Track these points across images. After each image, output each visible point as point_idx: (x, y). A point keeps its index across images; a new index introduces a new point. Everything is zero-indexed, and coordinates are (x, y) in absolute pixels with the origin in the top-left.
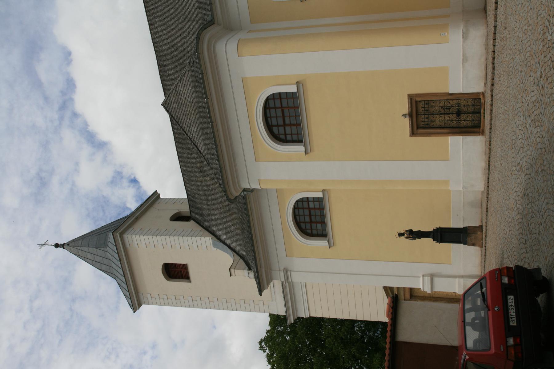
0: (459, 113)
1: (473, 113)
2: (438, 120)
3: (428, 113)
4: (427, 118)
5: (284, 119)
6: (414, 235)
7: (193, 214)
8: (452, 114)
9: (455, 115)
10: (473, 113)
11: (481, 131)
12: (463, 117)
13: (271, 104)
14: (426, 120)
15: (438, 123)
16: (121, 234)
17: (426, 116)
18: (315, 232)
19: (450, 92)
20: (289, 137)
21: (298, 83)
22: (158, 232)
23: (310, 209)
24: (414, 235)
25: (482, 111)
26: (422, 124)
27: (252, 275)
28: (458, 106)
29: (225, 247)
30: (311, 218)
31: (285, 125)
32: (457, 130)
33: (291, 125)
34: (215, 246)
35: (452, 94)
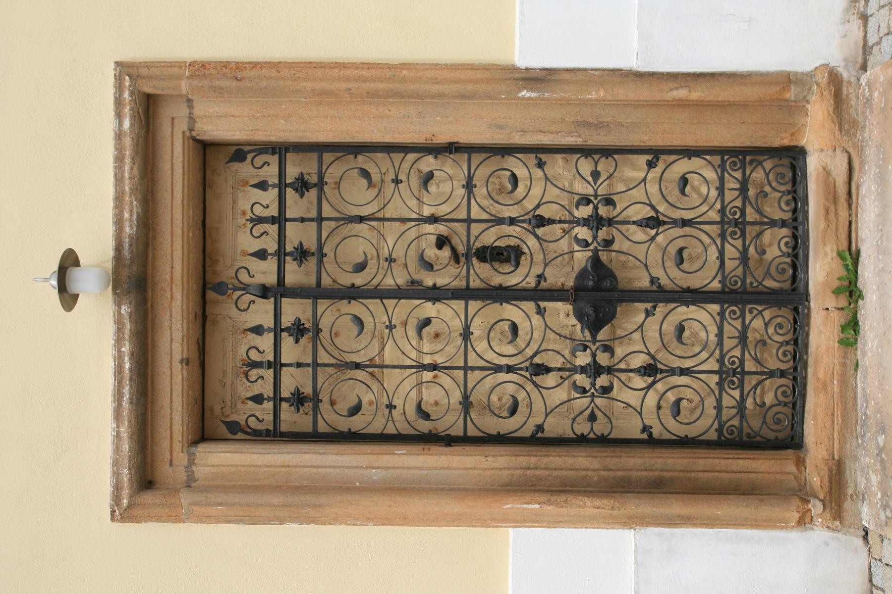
0: (599, 296)
1: (733, 296)
2: (409, 356)
3: (313, 287)
4: (298, 330)
8: (539, 294)
9: (562, 314)
10: (733, 296)
11: (816, 479)
12: (639, 333)
14: (290, 351)
15: (403, 389)
17: (294, 310)
19: (528, 55)
25: (821, 270)
26: (243, 394)
28: (596, 222)
31: (469, 221)
32: (582, 461)
35: (540, 78)
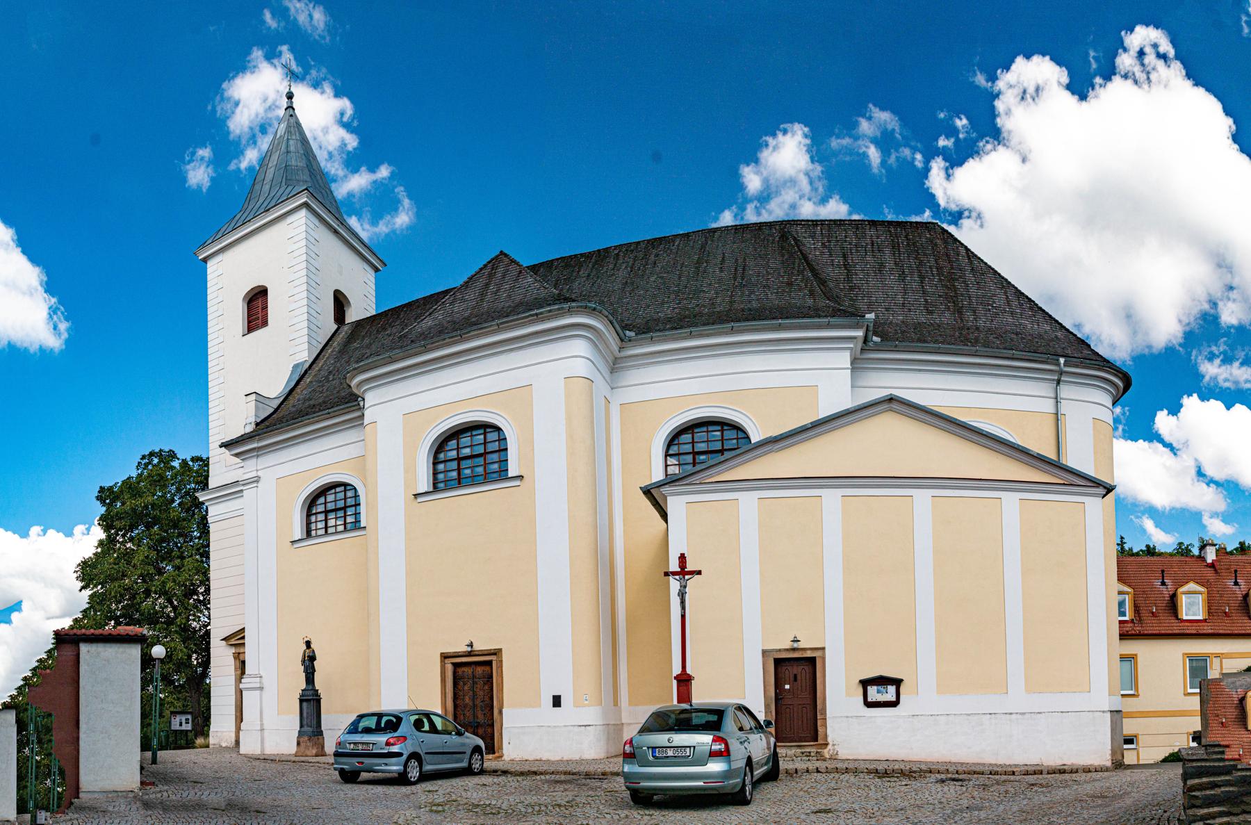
5: (469, 456)
6: (309, 661)
7: (346, 328)
13: (492, 436)
16: (306, 205)
18: (313, 519)
19: (504, 711)
20: (441, 467)
21: (521, 477)
22: (312, 271)
23: (344, 508)
24: (309, 661)
27: (249, 429)
29: (293, 384)
30: (340, 509)
33: (459, 470)
34: (296, 367)
